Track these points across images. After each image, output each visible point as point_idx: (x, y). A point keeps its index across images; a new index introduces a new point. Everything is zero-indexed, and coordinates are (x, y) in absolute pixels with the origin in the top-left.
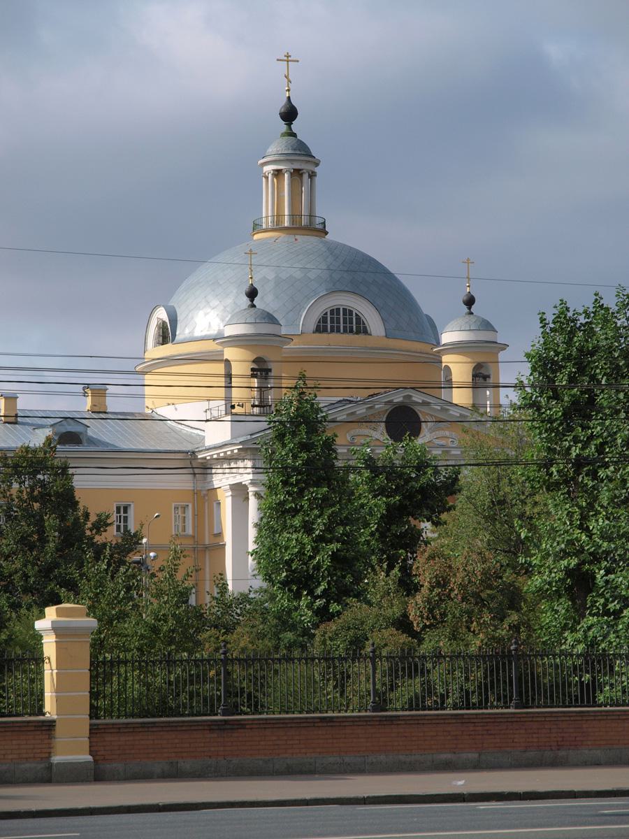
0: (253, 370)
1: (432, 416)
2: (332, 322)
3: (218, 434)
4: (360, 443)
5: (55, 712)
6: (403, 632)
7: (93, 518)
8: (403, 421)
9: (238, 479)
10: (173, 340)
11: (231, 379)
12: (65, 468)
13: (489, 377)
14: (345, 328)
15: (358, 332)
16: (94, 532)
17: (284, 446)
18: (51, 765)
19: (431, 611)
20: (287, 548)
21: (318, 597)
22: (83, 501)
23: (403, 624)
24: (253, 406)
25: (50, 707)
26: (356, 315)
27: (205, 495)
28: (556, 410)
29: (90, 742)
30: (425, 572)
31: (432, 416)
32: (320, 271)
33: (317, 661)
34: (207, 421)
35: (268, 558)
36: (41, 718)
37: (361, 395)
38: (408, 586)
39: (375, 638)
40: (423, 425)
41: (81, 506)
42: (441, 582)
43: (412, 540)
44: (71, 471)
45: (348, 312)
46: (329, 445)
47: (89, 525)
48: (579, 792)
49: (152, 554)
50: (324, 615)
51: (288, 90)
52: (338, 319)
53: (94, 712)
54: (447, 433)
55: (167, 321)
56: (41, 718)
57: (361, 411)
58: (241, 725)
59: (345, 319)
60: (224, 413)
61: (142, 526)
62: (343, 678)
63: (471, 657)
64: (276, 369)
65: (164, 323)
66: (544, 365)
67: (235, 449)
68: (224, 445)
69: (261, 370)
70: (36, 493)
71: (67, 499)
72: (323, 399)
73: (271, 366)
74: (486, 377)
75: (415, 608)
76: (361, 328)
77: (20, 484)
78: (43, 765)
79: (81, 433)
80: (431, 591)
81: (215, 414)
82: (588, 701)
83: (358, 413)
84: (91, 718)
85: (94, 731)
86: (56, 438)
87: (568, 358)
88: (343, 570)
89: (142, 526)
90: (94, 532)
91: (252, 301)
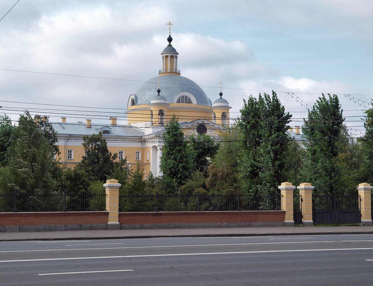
0: (159, 113)
1: (210, 127)
2: (182, 100)
3: (148, 132)
4: (190, 133)
5: (285, 209)
6: (204, 189)
7: (113, 155)
8: (202, 129)
9: (154, 144)
10: (136, 104)
11: (152, 116)
12: (105, 141)
13: (226, 116)
14: (185, 102)
15: (189, 103)
16: (113, 159)
17: (169, 135)
18: (107, 225)
19: (212, 183)
20: (170, 165)
21: (178, 179)
22: (110, 150)
23: (204, 186)
24: (159, 124)
25: (108, 208)
26: (189, 98)
27: (145, 149)
28: (249, 127)
29: (119, 219)
30: (211, 173)
31: (210, 127)
32: (178, 85)
33: (179, 197)
34: (146, 128)
35: (163, 167)
36: (105, 211)
37: (189, 121)
38: (206, 176)
39: (196, 190)
40: (208, 130)
41: (109, 152)
42: (215, 175)
43: (205, 162)
44: (106, 141)
45: (186, 97)
46: (182, 135)
47: (111, 157)
48: (257, 234)
49: (130, 166)
50: (180, 184)
51: (170, 33)
52: (183, 99)
53: (120, 210)
54: (214, 132)
55: (134, 98)
56: (105, 211)
57: (190, 125)
58: (161, 214)
59: (185, 99)
60: (150, 125)
61: (126, 157)
62: (186, 201)
63: (223, 196)
64: (165, 113)
65: (133, 99)
66: (246, 113)
67: (154, 136)
68: (150, 134)
69: (161, 113)
70: (96, 148)
71: (104, 149)
72: (180, 122)
73: (164, 112)
74: (225, 116)
75: (208, 181)
76: (190, 102)
77: (92, 145)
78: (105, 225)
79: (109, 131)
80: (212, 177)
81: (148, 126)
82: (222, 209)
83: (215, 126)
84: (119, 212)
85: (120, 215)
86: (102, 132)
87: (252, 111)
88: (186, 171)
89: (126, 157)
90: (113, 159)
91: (159, 93)
